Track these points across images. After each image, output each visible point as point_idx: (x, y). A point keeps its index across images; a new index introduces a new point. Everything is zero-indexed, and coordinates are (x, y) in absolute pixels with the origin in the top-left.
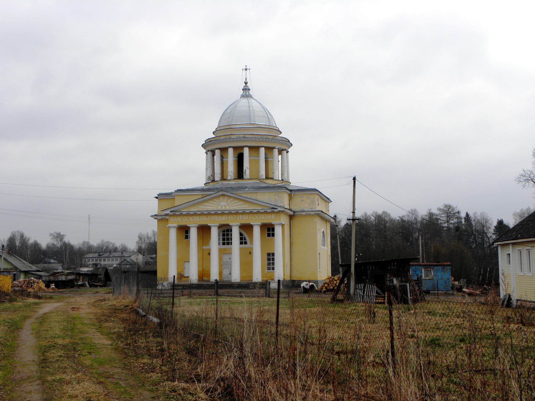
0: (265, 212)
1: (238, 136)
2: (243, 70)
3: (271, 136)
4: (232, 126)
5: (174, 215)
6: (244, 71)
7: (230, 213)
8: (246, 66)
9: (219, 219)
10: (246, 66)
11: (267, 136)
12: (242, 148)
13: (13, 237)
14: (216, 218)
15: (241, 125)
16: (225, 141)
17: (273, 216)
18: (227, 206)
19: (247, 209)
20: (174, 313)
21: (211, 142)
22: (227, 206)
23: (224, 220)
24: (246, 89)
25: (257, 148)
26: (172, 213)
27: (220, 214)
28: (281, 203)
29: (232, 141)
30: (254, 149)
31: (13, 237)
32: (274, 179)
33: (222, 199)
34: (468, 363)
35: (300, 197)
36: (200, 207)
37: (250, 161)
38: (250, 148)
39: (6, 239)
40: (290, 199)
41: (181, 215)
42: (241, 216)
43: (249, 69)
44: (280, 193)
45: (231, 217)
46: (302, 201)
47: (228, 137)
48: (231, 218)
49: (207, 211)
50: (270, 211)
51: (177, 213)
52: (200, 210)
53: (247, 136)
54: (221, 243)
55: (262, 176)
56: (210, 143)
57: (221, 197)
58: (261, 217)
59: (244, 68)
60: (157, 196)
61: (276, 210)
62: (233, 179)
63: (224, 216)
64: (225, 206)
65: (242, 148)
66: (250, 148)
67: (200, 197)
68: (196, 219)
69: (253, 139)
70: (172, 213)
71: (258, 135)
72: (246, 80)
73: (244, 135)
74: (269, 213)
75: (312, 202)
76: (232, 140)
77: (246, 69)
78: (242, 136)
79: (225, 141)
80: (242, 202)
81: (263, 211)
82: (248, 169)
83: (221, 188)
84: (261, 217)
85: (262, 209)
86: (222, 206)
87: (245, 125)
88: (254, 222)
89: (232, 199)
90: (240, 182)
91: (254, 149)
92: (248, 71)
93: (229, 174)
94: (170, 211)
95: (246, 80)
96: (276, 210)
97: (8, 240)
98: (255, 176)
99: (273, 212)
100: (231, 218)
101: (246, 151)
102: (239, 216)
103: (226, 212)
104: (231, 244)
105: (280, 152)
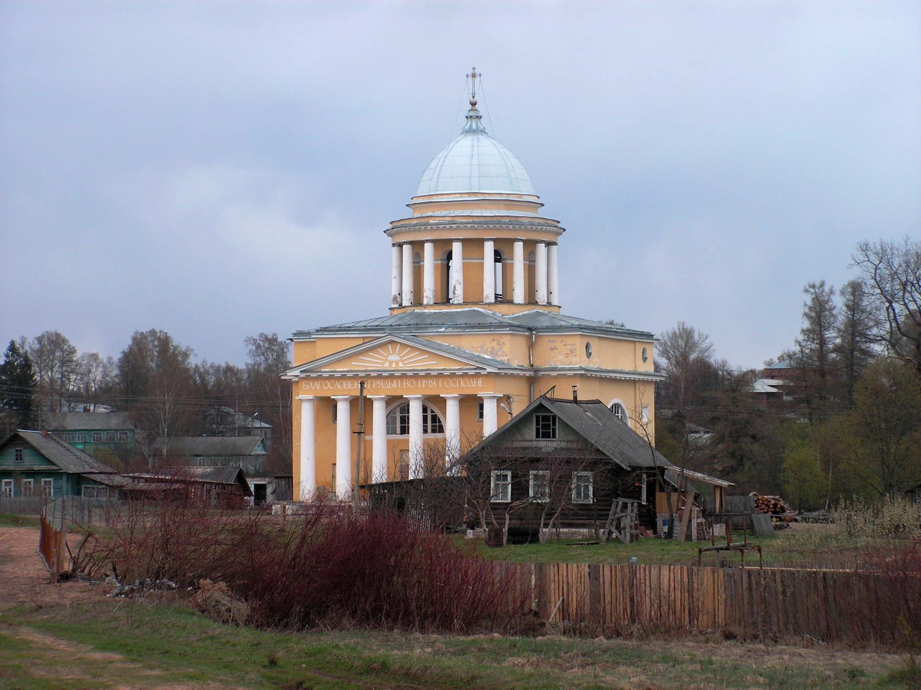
0: (465, 375)
1: (441, 219)
2: (467, 76)
3: (506, 218)
4: (435, 197)
5: (307, 378)
6: (470, 79)
7: (404, 376)
8: (474, 68)
9: (386, 386)
10: (474, 68)
11: (499, 218)
12: (450, 242)
13: (140, 350)
14: (380, 383)
15: (451, 196)
16: (416, 228)
17: (480, 382)
18: (400, 363)
19: (435, 368)
20: (717, 648)
21: (395, 230)
22: (400, 363)
23: (394, 388)
24: (471, 117)
25: (480, 242)
26: (303, 375)
27: (386, 377)
28: (503, 356)
29: (430, 230)
30: (473, 245)
31: (140, 350)
32: (515, 302)
33: (391, 349)
34: (90, 512)
35: (549, 341)
36: (353, 363)
37: (465, 267)
38: (464, 241)
39: (117, 356)
40: (531, 346)
41: (319, 378)
42: (424, 381)
43: (480, 75)
44: (501, 338)
45: (407, 384)
46: (552, 349)
47: (423, 221)
48: (406, 385)
49: (364, 371)
50: (472, 372)
51: (313, 375)
52: (353, 369)
53: (457, 220)
54: (429, 429)
55: (487, 297)
56: (392, 230)
57: (389, 345)
58: (459, 385)
59: (470, 72)
60: (291, 337)
61: (483, 372)
62: (432, 303)
63: (395, 381)
64: (397, 363)
65: (450, 242)
66: (464, 241)
67: (361, 342)
68: (347, 386)
69: (469, 226)
70: (303, 375)
71: (481, 218)
72: (473, 97)
73: (453, 218)
74: (473, 375)
75: (571, 351)
76: (429, 227)
77: (474, 76)
78: (448, 219)
79: (416, 228)
80: (426, 356)
81: (460, 373)
82: (460, 284)
83: (399, 325)
84: (459, 385)
85: (459, 370)
86: (391, 363)
87: (458, 195)
88: (447, 394)
89: (409, 349)
90: (445, 309)
91: (473, 245)
92: (478, 78)
93: (425, 294)
94: (301, 371)
95: (473, 97)
96: (483, 372)
97: (120, 360)
98: (473, 296)
99: (477, 375)
100: (406, 385)
101: (457, 248)
102: (421, 381)
103: (397, 374)
104: (408, 433)
105: (549, 244)
